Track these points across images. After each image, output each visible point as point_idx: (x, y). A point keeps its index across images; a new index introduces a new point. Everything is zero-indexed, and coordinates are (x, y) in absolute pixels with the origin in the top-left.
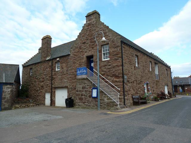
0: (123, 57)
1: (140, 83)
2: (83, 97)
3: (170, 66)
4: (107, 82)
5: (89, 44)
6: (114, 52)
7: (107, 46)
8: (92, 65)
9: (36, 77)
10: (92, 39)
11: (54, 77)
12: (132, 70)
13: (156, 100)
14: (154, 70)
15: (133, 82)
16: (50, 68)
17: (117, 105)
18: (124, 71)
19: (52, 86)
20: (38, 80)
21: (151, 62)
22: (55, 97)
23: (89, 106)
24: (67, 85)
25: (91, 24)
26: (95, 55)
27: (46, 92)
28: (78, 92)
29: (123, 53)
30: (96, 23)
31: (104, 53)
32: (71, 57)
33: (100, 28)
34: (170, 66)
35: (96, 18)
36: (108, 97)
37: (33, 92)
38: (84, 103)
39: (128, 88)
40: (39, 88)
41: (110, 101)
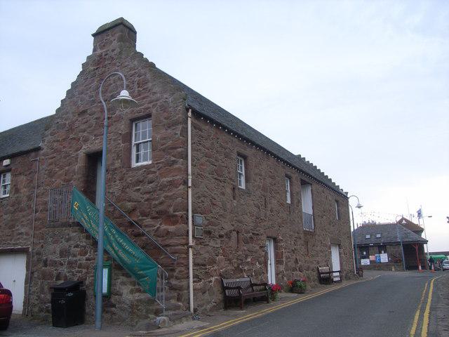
3: (347, 193)
6: (165, 138)
7: (148, 123)
15: (226, 234)
25: (107, 57)
30: (120, 53)
31: (138, 145)
32: (44, 155)
34: (347, 193)
35: (121, 39)
39: (207, 256)
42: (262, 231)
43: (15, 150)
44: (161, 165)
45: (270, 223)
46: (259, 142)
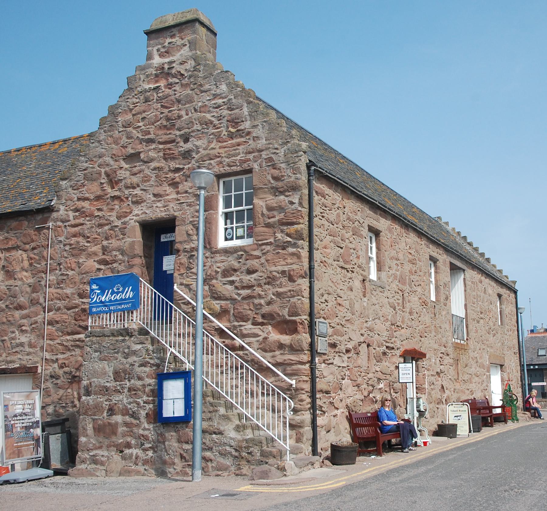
1: (384, 354)
2: (118, 418)
3: (515, 282)
5: (153, 165)
12: (352, 295)
14: (447, 298)
15: (355, 348)
17: (281, 454)
18: (316, 299)
21: (434, 260)
30: (195, 69)
33: (215, 96)
34: (515, 282)
39: (330, 378)
41: (249, 434)
46: (398, 209)
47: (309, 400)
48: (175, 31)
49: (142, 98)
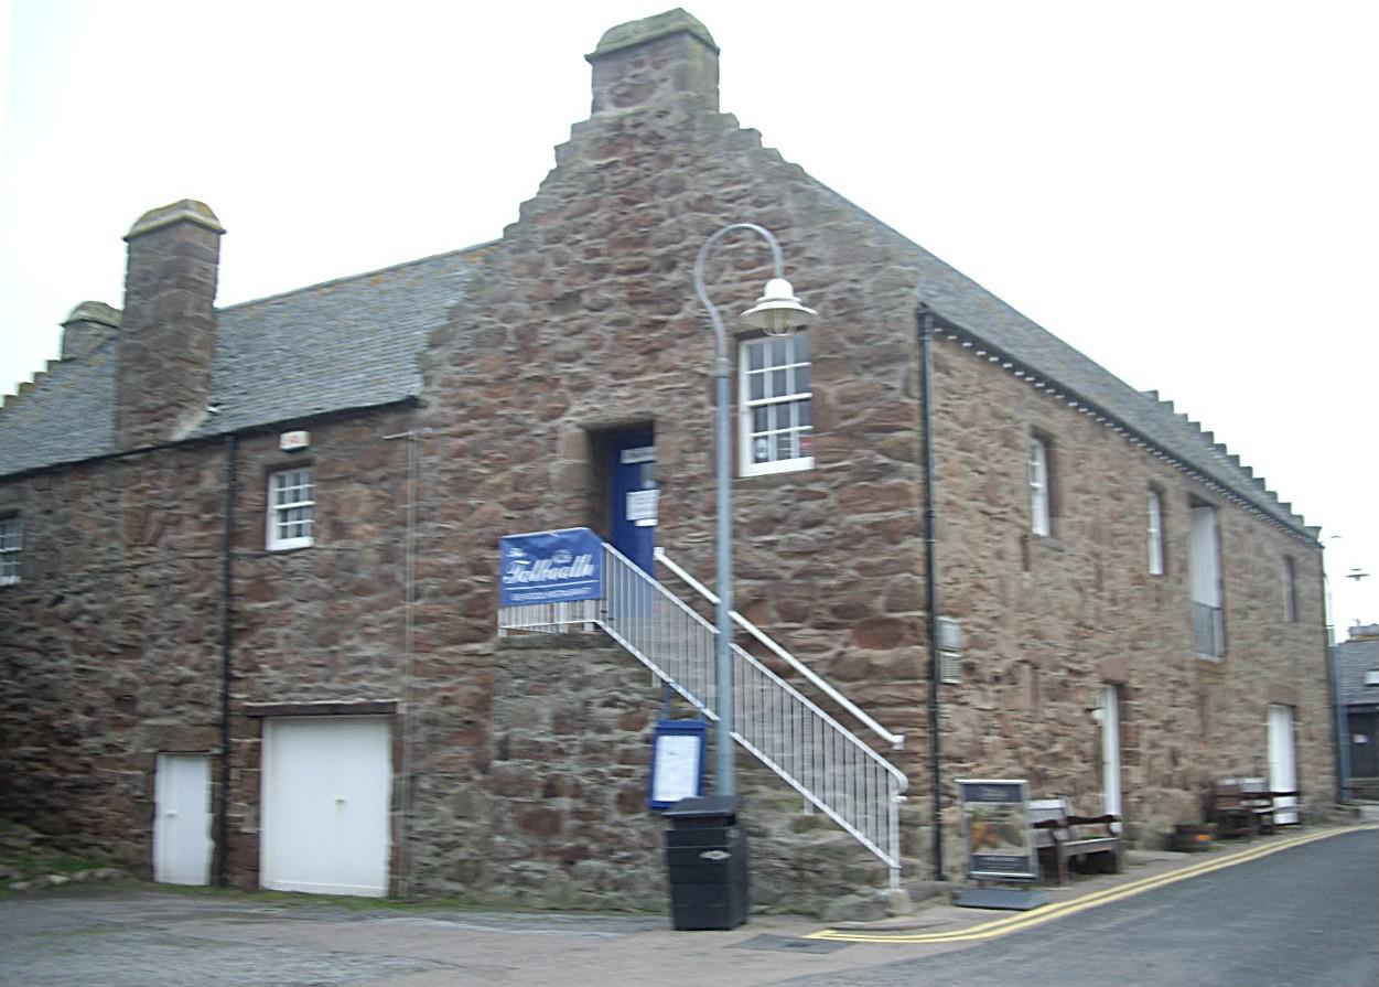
0: (934, 456)
2: (564, 803)
4: (786, 672)
5: (611, 314)
8: (642, 508)
9: (60, 599)
10: (645, 269)
11: (250, 606)
13: (1179, 841)
14: (1184, 568)
15: (1009, 673)
16: (207, 525)
17: (877, 877)
18: (939, 578)
19: (225, 698)
20: (78, 631)
21: (1157, 490)
22: (256, 803)
23: (617, 885)
24: (393, 689)
25: (641, 132)
26: (670, 423)
27: (171, 747)
28: (515, 762)
29: (933, 419)
30: (688, 125)
33: (729, 180)
34: (1318, 529)
36: (800, 802)
37: (27, 750)
38: (570, 859)
40: (90, 711)
42: (1090, 665)
43: (331, 401)
44: (842, 477)
45: (1112, 635)
47: (927, 775)
48: (644, 54)
49: (582, 184)
